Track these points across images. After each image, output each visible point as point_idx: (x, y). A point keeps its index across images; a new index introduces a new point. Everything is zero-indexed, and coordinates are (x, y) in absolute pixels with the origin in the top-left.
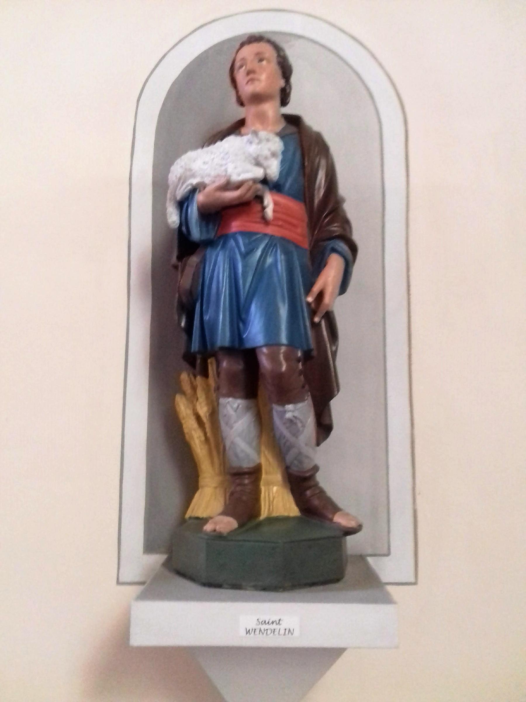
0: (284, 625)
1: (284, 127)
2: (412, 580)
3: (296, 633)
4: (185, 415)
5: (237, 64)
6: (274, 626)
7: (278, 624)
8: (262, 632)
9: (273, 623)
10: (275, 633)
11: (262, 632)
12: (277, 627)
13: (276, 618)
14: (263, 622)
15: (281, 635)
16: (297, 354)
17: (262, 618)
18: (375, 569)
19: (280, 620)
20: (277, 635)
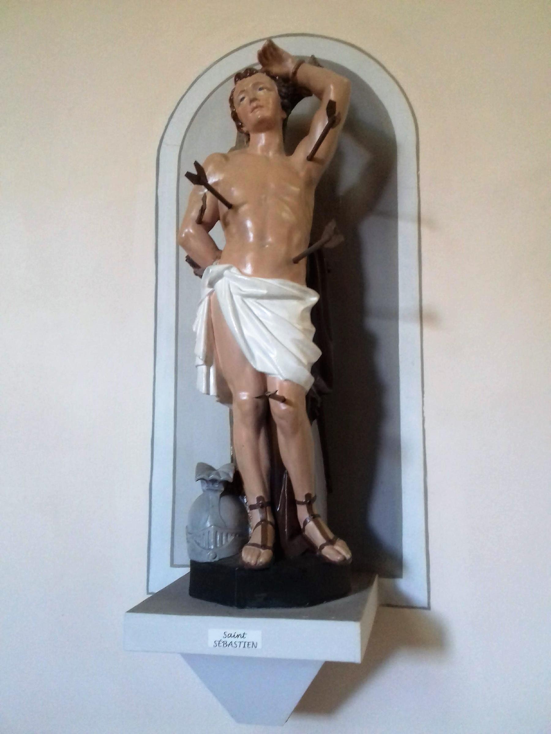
0: (248, 639)
1: (323, 549)
2: (176, 562)
3: (259, 646)
4: (267, 508)
5: (237, 98)
6: (239, 639)
7: (233, 637)
8: (255, 646)
9: (238, 636)
10: (249, 646)
11: (255, 646)
12: (242, 640)
13: (241, 632)
14: (229, 636)
15: (250, 647)
16: (182, 235)
17: (229, 632)
18: (186, 551)
19: (244, 634)
20: (251, 648)
